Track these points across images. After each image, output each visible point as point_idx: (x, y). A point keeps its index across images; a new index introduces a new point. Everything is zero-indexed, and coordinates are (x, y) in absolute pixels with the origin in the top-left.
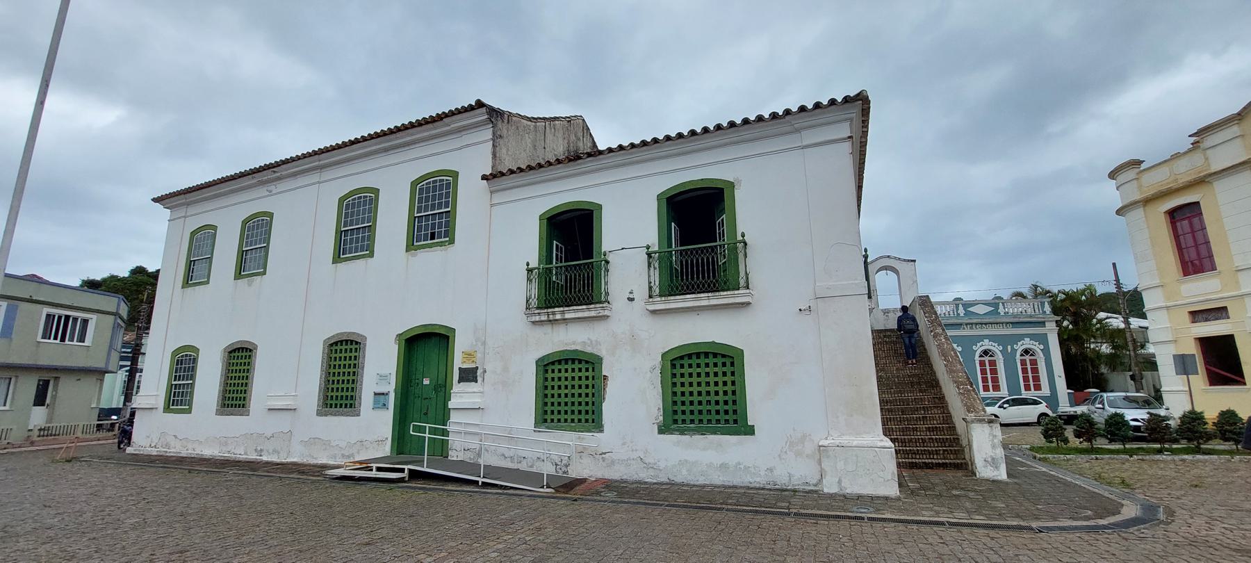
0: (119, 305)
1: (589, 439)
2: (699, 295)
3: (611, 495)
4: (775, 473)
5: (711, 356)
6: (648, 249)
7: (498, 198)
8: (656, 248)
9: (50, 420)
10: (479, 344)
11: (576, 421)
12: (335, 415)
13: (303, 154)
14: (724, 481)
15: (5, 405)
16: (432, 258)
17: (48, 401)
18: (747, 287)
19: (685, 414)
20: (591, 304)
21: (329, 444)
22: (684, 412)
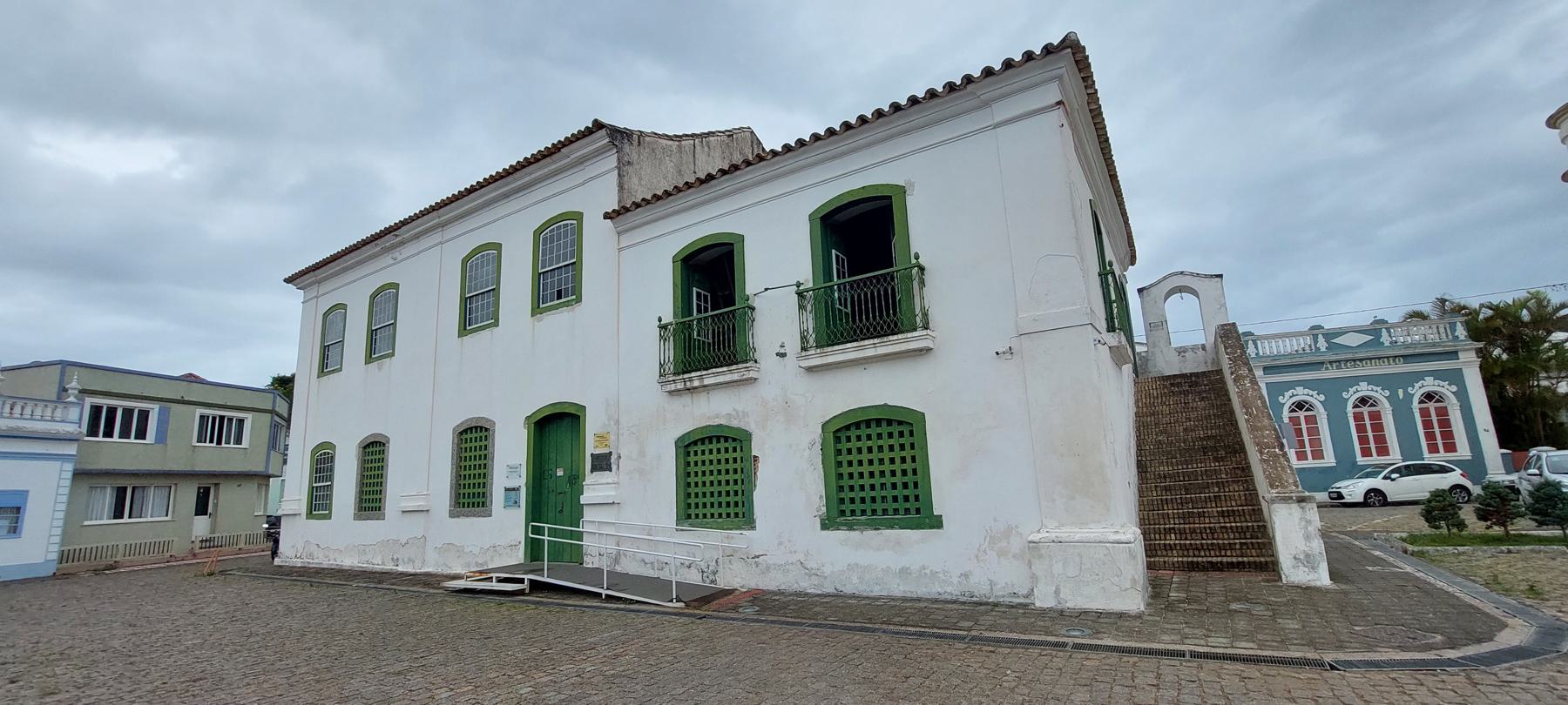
0: (274, 402)
1: (739, 539)
2: (862, 343)
3: (750, 611)
4: (973, 580)
5: (884, 424)
6: (798, 287)
7: (626, 240)
8: (811, 285)
9: (213, 531)
10: (612, 423)
11: (724, 515)
12: (467, 516)
13: (421, 211)
14: (905, 592)
15: (167, 515)
16: (558, 320)
17: (210, 510)
18: (926, 327)
19: (854, 503)
20: (732, 365)
21: (463, 550)
22: (852, 501)
